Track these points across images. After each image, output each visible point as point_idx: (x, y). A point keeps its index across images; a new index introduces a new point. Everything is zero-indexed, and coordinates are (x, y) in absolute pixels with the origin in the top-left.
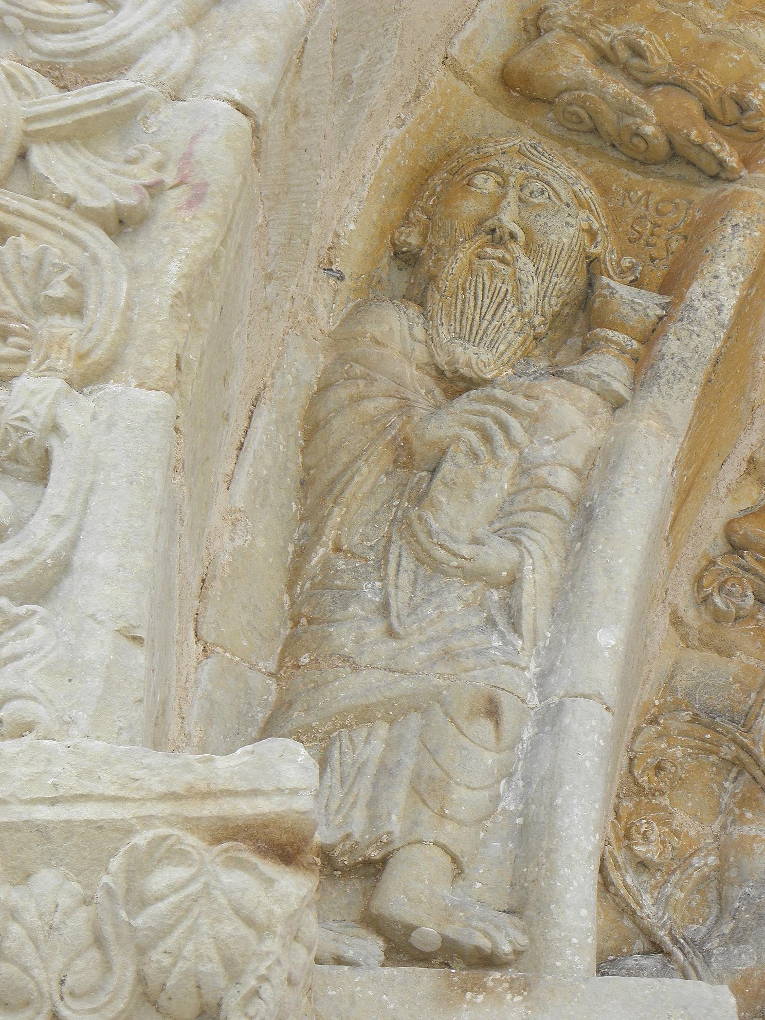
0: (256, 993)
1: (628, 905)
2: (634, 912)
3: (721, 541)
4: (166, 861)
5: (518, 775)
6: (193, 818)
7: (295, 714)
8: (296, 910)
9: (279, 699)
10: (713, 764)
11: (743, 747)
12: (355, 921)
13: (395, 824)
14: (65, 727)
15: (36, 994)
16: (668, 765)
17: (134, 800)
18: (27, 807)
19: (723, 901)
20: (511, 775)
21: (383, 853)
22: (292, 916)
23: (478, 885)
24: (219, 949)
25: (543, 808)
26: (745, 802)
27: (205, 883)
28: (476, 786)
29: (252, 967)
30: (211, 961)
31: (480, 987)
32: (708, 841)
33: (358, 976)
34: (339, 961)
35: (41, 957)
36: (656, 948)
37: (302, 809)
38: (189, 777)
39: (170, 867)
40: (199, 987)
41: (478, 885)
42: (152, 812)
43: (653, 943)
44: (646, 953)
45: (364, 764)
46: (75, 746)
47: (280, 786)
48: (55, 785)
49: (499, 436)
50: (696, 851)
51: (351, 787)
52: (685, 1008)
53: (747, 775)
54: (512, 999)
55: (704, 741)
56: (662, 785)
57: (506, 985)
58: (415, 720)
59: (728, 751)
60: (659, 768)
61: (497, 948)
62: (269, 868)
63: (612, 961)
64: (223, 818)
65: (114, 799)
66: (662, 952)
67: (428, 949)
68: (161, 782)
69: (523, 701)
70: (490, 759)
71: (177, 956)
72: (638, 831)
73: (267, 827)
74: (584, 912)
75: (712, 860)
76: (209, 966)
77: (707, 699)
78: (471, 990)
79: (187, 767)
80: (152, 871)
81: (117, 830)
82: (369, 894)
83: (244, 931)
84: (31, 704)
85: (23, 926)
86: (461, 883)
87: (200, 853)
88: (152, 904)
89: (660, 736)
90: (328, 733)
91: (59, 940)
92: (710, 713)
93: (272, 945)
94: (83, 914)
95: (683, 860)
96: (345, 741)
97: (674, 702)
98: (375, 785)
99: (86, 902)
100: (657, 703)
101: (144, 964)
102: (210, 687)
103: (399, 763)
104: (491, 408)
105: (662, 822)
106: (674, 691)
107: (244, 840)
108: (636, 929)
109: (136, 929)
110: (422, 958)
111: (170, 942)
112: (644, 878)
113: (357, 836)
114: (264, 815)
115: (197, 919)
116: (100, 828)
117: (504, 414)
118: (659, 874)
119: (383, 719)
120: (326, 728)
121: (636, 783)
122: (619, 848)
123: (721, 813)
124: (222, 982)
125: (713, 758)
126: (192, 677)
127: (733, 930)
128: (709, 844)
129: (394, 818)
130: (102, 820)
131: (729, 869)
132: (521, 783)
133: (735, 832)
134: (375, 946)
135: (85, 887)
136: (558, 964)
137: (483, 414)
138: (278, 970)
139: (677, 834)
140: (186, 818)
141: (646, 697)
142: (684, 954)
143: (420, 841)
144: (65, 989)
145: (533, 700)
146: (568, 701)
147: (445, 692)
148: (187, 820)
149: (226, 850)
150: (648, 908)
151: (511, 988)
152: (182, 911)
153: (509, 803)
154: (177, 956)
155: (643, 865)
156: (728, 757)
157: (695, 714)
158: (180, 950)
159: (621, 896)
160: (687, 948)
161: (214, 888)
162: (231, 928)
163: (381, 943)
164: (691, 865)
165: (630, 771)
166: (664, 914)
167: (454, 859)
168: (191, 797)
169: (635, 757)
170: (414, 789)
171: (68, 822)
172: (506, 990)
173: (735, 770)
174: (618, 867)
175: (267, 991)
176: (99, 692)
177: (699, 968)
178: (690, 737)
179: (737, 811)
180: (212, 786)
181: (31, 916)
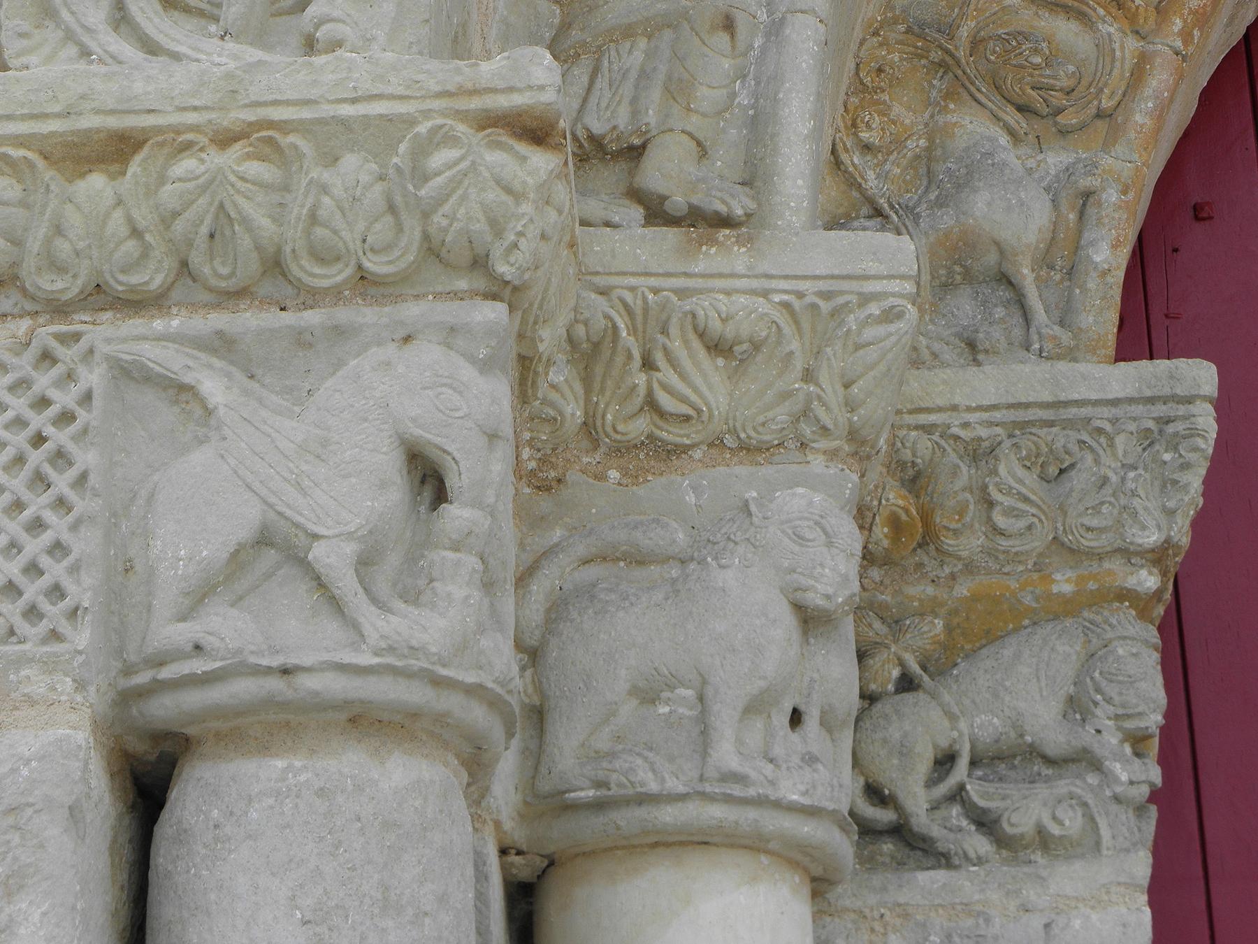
0: (515, 245)
1: (855, 179)
2: (860, 185)
4: (442, 145)
5: (751, 76)
6: (462, 111)
7: (574, 33)
8: (545, 181)
9: (562, 21)
10: (924, 66)
11: (947, 51)
12: (622, 194)
13: (651, 117)
14: (367, 43)
15: (344, 251)
16: (887, 68)
17: (416, 98)
18: (333, 106)
19: (931, 174)
20: (745, 76)
21: (642, 140)
22: (542, 185)
23: (719, 163)
24: (485, 212)
25: (769, 101)
26: (948, 95)
27: (472, 161)
28: (715, 85)
29: (511, 225)
30: (479, 221)
31: (712, 241)
32: (919, 127)
33: (617, 235)
34: (608, 224)
35: (347, 222)
36: (878, 213)
37: (548, 101)
38: (458, 79)
39: (446, 149)
40: (470, 242)
41: (719, 163)
42: (430, 107)
43: (876, 209)
44: (870, 217)
45: (628, 70)
46: (370, 57)
47: (530, 84)
48: (354, 88)
50: (909, 136)
51: (617, 89)
52: (874, 254)
53: (951, 74)
54: (738, 250)
55: (917, 48)
56: (882, 84)
57: (733, 239)
58: (668, 34)
59: (936, 55)
60: (880, 70)
61: (732, 212)
62: (523, 148)
63: (842, 224)
64: (486, 110)
65: (401, 98)
66: (882, 215)
67: (679, 214)
68: (437, 83)
69: (754, 17)
70: (726, 64)
71: (452, 218)
72: (862, 121)
73: (520, 116)
74: (800, 182)
75: (923, 142)
76: (478, 225)
77: (919, 15)
78: (706, 244)
79: (458, 71)
80: (432, 153)
81: (404, 122)
82: (632, 173)
83: (504, 197)
84: (340, 26)
85: (332, 198)
86: (706, 162)
87: (468, 138)
88: (432, 179)
89: (881, 45)
90: (599, 47)
91: (360, 208)
92: (922, 26)
93: (527, 208)
94: (378, 187)
95: (899, 143)
96: (613, 53)
97: (892, 18)
98: (636, 87)
99: (382, 178)
100: (879, 18)
101: (428, 226)
102: (505, 13)
103: (655, 69)
105: (882, 114)
106: (893, 8)
107: (502, 127)
108: (862, 199)
109: (421, 198)
110: (673, 221)
111: (446, 208)
112: (869, 158)
113: (622, 127)
114: (519, 107)
115: (467, 189)
116: (390, 120)
118: (880, 154)
119: (642, 34)
120: (598, 43)
121: (862, 83)
122: (848, 135)
123: (930, 105)
124: (489, 238)
125: (923, 61)
126: (491, 5)
127: (937, 197)
128: (921, 130)
129: (651, 112)
130: (391, 114)
131: (935, 149)
132: (753, 83)
133: (941, 120)
134: (637, 213)
135: (381, 167)
136: (779, 223)
138: (532, 227)
139: (894, 122)
140: (457, 110)
141: (870, 14)
142: (898, 217)
143: (672, 130)
144: (366, 246)
145: (763, 16)
146: (789, 16)
147: (691, 12)
148: (457, 112)
149: (488, 136)
150: (871, 181)
151: (737, 242)
152: (456, 183)
153: (744, 99)
154: (452, 218)
155: (867, 148)
156: (936, 60)
157: (909, 27)
158: (455, 214)
159: (850, 173)
160: (901, 212)
161: (480, 165)
162: (493, 195)
163: (642, 211)
164: (906, 147)
165: (857, 74)
166: (884, 186)
167: (699, 144)
168: (461, 94)
169: (861, 62)
170: (667, 89)
171: (364, 116)
172: (733, 244)
173: (942, 70)
174: (847, 150)
175: (523, 243)
176: (393, 15)
177: (910, 228)
178: (905, 45)
179: (942, 103)
180: (477, 85)
181: (338, 191)
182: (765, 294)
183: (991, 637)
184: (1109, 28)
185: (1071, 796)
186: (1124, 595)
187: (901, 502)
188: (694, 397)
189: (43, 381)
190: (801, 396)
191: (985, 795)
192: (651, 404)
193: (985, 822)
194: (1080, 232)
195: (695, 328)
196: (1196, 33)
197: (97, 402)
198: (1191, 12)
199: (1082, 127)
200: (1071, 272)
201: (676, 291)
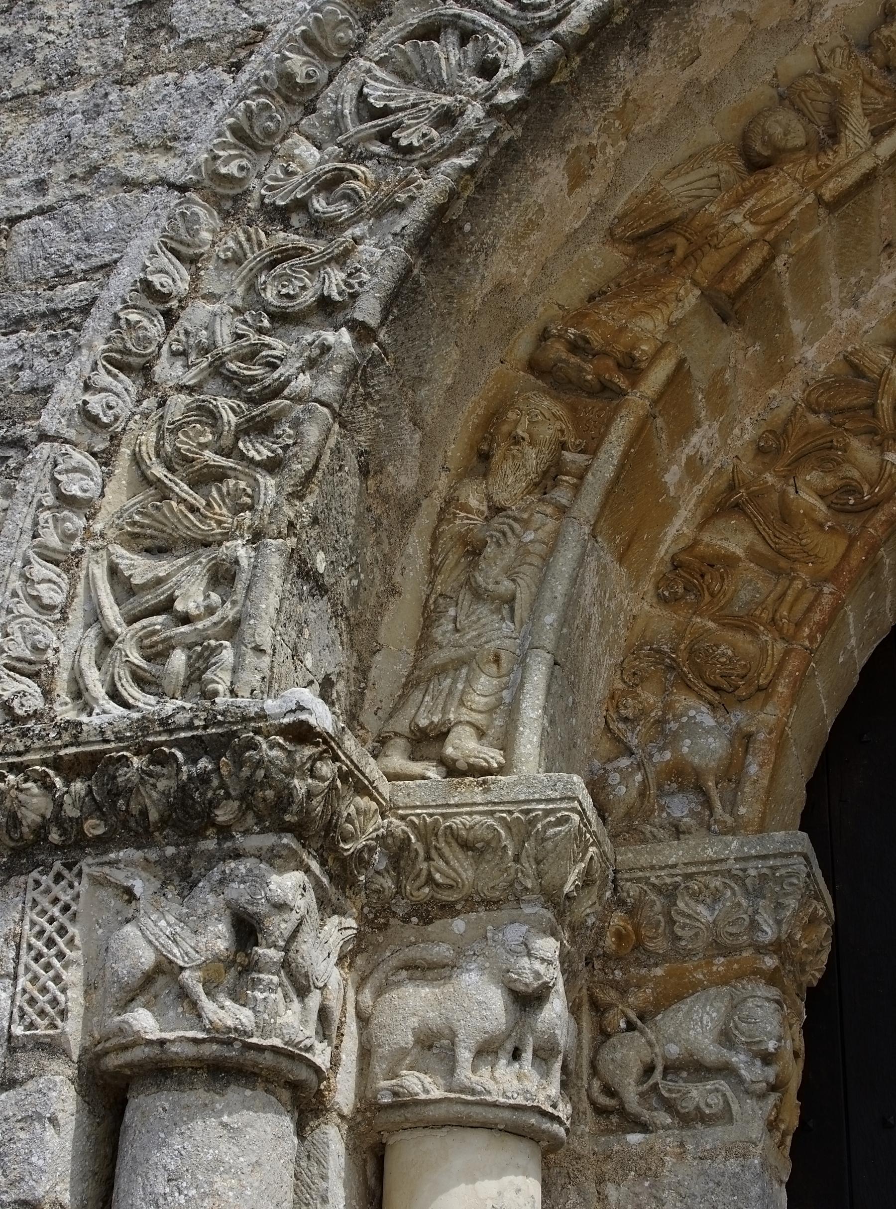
3: (669, 565)
49: (509, 534)
104: (506, 521)
110: (464, 774)
117: (511, 521)
137: (503, 523)
155: (626, 720)
182: (492, 813)
183: (680, 998)
184: (767, 638)
185: (717, 1090)
186: (757, 972)
187: (622, 923)
188: (453, 875)
189: (57, 890)
190: (512, 871)
191: (670, 1091)
192: (430, 880)
193: (669, 1106)
194: (745, 758)
195: (453, 836)
196: (819, 636)
197: (81, 899)
198: (814, 623)
199: (750, 697)
200: (738, 783)
201: (442, 815)
